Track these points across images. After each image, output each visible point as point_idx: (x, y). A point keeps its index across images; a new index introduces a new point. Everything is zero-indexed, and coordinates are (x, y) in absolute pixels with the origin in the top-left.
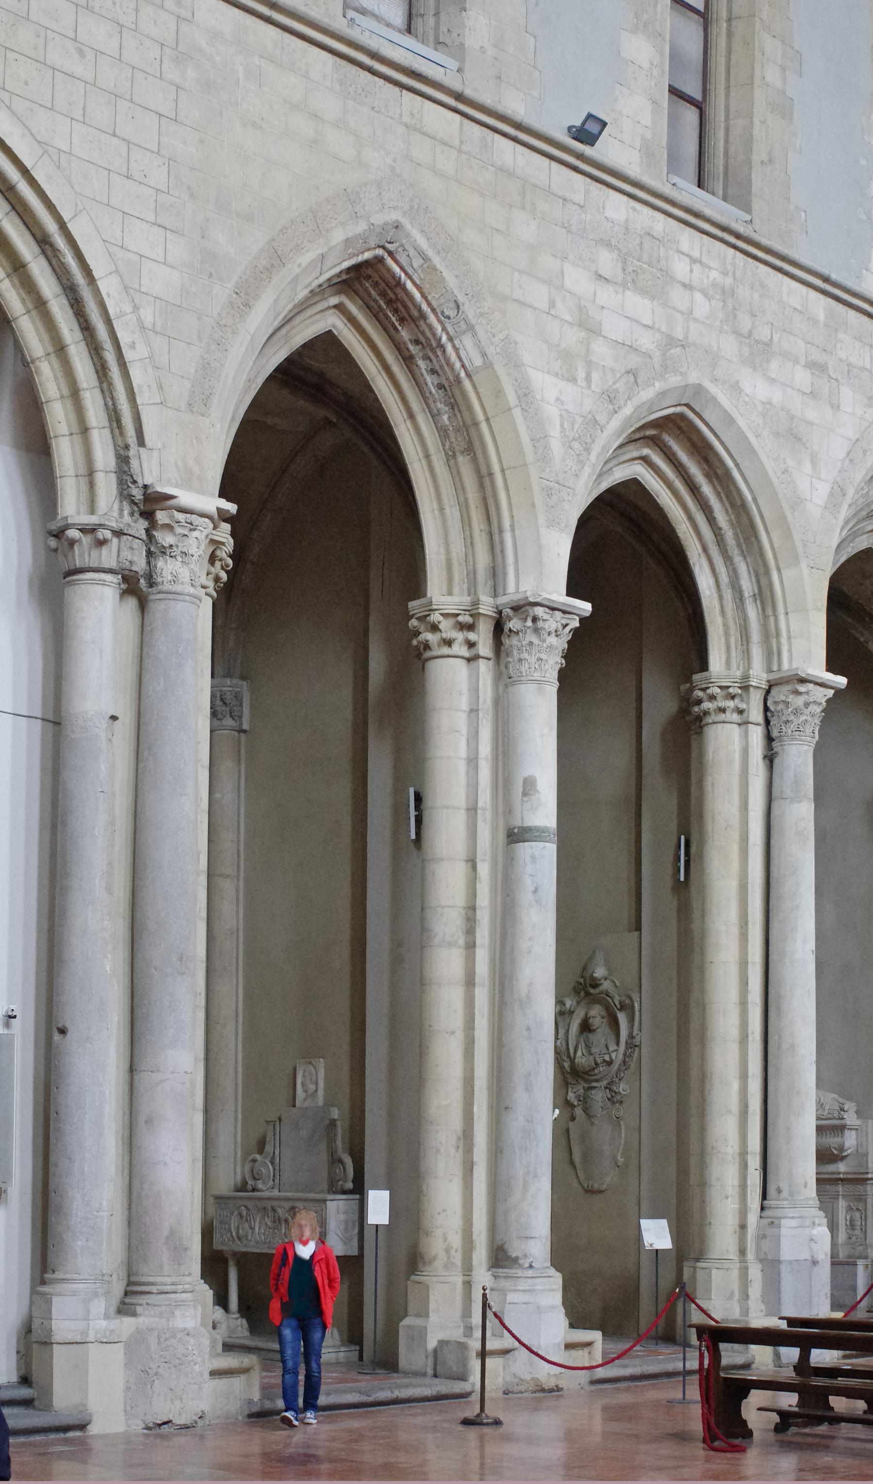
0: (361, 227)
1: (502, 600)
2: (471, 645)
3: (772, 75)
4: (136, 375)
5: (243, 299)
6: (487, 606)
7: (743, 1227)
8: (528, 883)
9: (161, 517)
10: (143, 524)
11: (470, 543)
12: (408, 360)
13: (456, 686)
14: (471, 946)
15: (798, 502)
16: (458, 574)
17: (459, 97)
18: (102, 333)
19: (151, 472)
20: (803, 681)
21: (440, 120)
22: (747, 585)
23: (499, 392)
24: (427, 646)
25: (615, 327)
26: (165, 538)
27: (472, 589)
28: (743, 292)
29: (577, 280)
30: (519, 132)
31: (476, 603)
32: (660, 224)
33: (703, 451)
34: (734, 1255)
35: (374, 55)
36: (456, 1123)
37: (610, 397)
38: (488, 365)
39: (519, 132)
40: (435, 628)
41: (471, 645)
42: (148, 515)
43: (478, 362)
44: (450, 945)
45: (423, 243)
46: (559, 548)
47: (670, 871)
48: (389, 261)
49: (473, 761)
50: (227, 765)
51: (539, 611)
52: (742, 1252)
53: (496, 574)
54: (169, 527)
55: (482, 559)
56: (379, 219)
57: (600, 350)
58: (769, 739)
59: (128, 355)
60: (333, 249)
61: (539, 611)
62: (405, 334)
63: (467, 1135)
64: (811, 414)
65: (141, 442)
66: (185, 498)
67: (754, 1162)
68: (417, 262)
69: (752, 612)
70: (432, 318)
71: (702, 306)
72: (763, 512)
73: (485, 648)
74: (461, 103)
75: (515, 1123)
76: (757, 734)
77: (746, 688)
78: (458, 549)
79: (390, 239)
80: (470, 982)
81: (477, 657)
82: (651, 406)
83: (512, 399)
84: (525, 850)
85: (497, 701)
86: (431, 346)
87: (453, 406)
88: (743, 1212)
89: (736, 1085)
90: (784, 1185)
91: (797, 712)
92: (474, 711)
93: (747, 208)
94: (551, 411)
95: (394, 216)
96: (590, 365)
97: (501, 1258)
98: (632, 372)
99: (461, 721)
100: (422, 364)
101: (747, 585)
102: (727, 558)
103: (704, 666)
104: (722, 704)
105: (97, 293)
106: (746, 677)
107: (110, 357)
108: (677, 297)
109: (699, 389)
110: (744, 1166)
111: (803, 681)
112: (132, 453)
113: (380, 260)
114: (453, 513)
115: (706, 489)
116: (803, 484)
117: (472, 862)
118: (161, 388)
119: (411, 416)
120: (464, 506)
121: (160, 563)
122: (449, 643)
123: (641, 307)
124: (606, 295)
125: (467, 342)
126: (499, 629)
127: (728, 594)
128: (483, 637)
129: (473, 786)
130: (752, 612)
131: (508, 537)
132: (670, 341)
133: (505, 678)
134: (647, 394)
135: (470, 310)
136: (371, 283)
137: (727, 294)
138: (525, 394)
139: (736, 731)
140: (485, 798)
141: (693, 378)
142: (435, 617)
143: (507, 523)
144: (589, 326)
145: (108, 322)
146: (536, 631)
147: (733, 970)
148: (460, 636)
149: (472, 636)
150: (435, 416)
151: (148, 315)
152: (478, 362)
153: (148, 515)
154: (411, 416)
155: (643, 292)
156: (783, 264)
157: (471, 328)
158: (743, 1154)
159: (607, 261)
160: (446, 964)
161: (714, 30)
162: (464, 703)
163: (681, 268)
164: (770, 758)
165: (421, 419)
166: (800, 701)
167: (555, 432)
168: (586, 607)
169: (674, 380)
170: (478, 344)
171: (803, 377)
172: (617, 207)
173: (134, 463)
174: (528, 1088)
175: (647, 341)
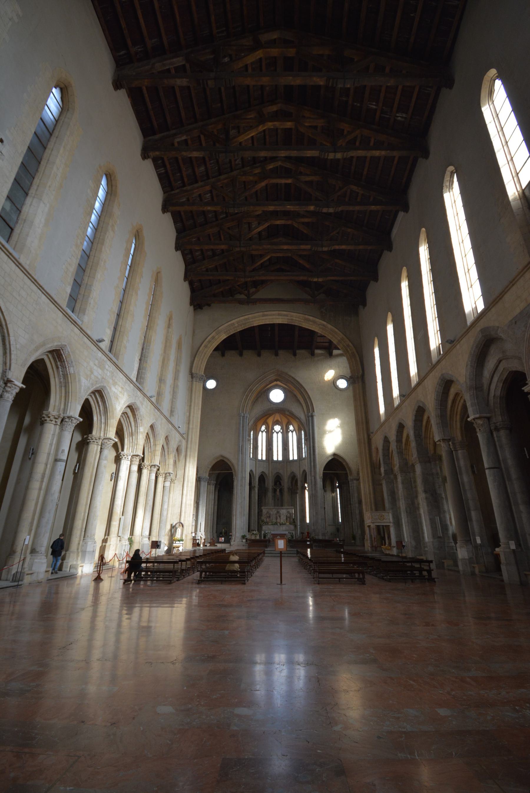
0: (60, 344)
1: (65, 415)
2: (56, 422)
3: (125, 342)
4: (13, 357)
5: (36, 349)
6: (62, 416)
7: (79, 544)
8: (59, 470)
9: (9, 385)
10: (4, 385)
11: (60, 403)
12: (57, 368)
13: (50, 430)
14: (42, 482)
15: (116, 409)
16: (56, 408)
17: (81, 328)
18: (8, 346)
19: (10, 375)
20: (111, 439)
21: (77, 331)
22: (103, 421)
23: (75, 378)
24: (46, 420)
25: (96, 373)
26: (8, 389)
27: (59, 411)
28: (115, 373)
29: (91, 363)
30: (89, 337)
31: (60, 414)
32: (105, 359)
33: (102, 397)
34: (76, 550)
35: (69, 316)
36: (30, 520)
37: (92, 384)
38: (74, 373)
39: (89, 337)
40: (49, 417)
41: (56, 422)
42: (6, 384)
43: (73, 372)
44: (38, 481)
45: (69, 350)
46: (79, 408)
47: (73, 468)
48: (61, 351)
49: (51, 445)
50: (204, 485)
51: (73, 419)
52: (78, 549)
53: (65, 410)
54: (10, 387)
55: (62, 406)
56: (63, 343)
57: (92, 376)
58: (101, 448)
59: (12, 352)
60: (50, 346)
61: (73, 419)
62: (59, 363)
63: (32, 523)
64: (120, 395)
65: (10, 369)
66: (16, 383)
67: (84, 530)
68: (67, 353)
69: (103, 426)
70: (66, 363)
71: (109, 374)
72: (109, 409)
73: (59, 423)
74: (81, 329)
75: (44, 521)
76: (99, 447)
77: (99, 439)
78: (57, 404)
79: (63, 347)
80: (40, 489)
81: (57, 424)
82: (97, 388)
83: (77, 380)
84: (59, 463)
85: (59, 433)
86: (64, 367)
87: (64, 378)
88: (80, 541)
89: (83, 514)
90: (89, 535)
91: (108, 444)
92: (54, 435)
93: (118, 360)
94: (83, 384)
95: (66, 344)
96: (90, 378)
97: (33, 551)
98: (96, 381)
99: (50, 436)
100: (60, 369)
101: (103, 421)
102: (101, 415)
103: (91, 432)
104: (94, 440)
105: (9, 339)
106: (100, 437)
107: (8, 351)
108: (105, 371)
109: (105, 387)
110: (82, 531)
111: (111, 439)
112: (7, 371)
113: (59, 350)
114: (58, 397)
115: (100, 403)
116: (117, 406)
117: (46, 465)
118: (17, 360)
119: (55, 378)
120: (61, 397)
121: (5, 394)
122: (52, 421)
123: (100, 371)
124: (95, 368)
125: (72, 368)
126: (62, 421)
127: (99, 422)
128: (59, 421)
129: (50, 449)
130: (103, 426)
131: (69, 404)
132: (103, 378)
133: (62, 429)
134: (98, 386)
135: (74, 363)
136: (57, 354)
137: (112, 373)
138: (79, 380)
139: (96, 446)
140: (52, 452)
141: (105, 385)
142: (50, 415)
143: (70, 401)
144: (92, 373)
145: (10, 345)
146: (71, 422)
147: (87, 491)
148: (54, 420)
149: (57, 420)
150: (60, 379)
151: (18, 346)
152: (73, 372)
153: (6, 384)
154: (55, 378)
155: (101, 369)
156: (121, 371)
157: (73, 367)
158: (82, 528)
159: (97, 362)
160: (35, 485)
161: (117, 332)
162: (52, 433)
163: (107, 367)
164: (101, 452)
165: (56, 379)
166: (109, 443)
167: (83, 388)
168: (81, 420)
169: (102, 384)
170: (74, 370)
171: (120, 389)
172: (100, 354)
173: (7, 373)
174: (49, 513)
175: (100, 377)
